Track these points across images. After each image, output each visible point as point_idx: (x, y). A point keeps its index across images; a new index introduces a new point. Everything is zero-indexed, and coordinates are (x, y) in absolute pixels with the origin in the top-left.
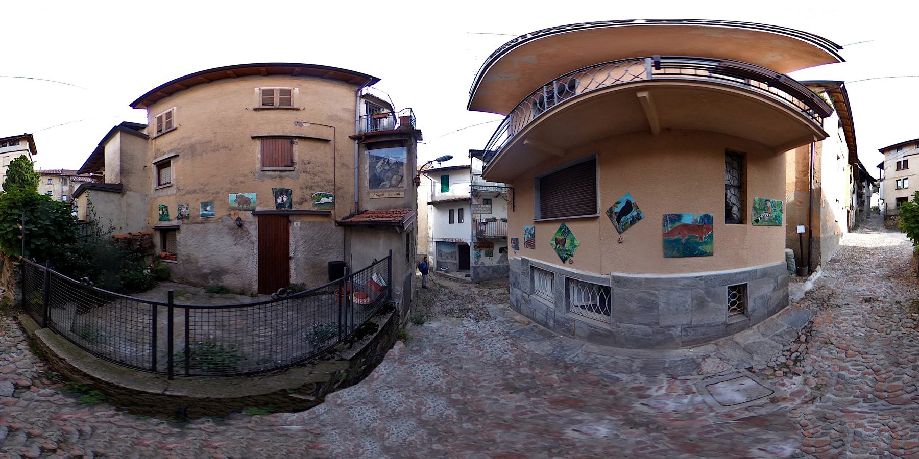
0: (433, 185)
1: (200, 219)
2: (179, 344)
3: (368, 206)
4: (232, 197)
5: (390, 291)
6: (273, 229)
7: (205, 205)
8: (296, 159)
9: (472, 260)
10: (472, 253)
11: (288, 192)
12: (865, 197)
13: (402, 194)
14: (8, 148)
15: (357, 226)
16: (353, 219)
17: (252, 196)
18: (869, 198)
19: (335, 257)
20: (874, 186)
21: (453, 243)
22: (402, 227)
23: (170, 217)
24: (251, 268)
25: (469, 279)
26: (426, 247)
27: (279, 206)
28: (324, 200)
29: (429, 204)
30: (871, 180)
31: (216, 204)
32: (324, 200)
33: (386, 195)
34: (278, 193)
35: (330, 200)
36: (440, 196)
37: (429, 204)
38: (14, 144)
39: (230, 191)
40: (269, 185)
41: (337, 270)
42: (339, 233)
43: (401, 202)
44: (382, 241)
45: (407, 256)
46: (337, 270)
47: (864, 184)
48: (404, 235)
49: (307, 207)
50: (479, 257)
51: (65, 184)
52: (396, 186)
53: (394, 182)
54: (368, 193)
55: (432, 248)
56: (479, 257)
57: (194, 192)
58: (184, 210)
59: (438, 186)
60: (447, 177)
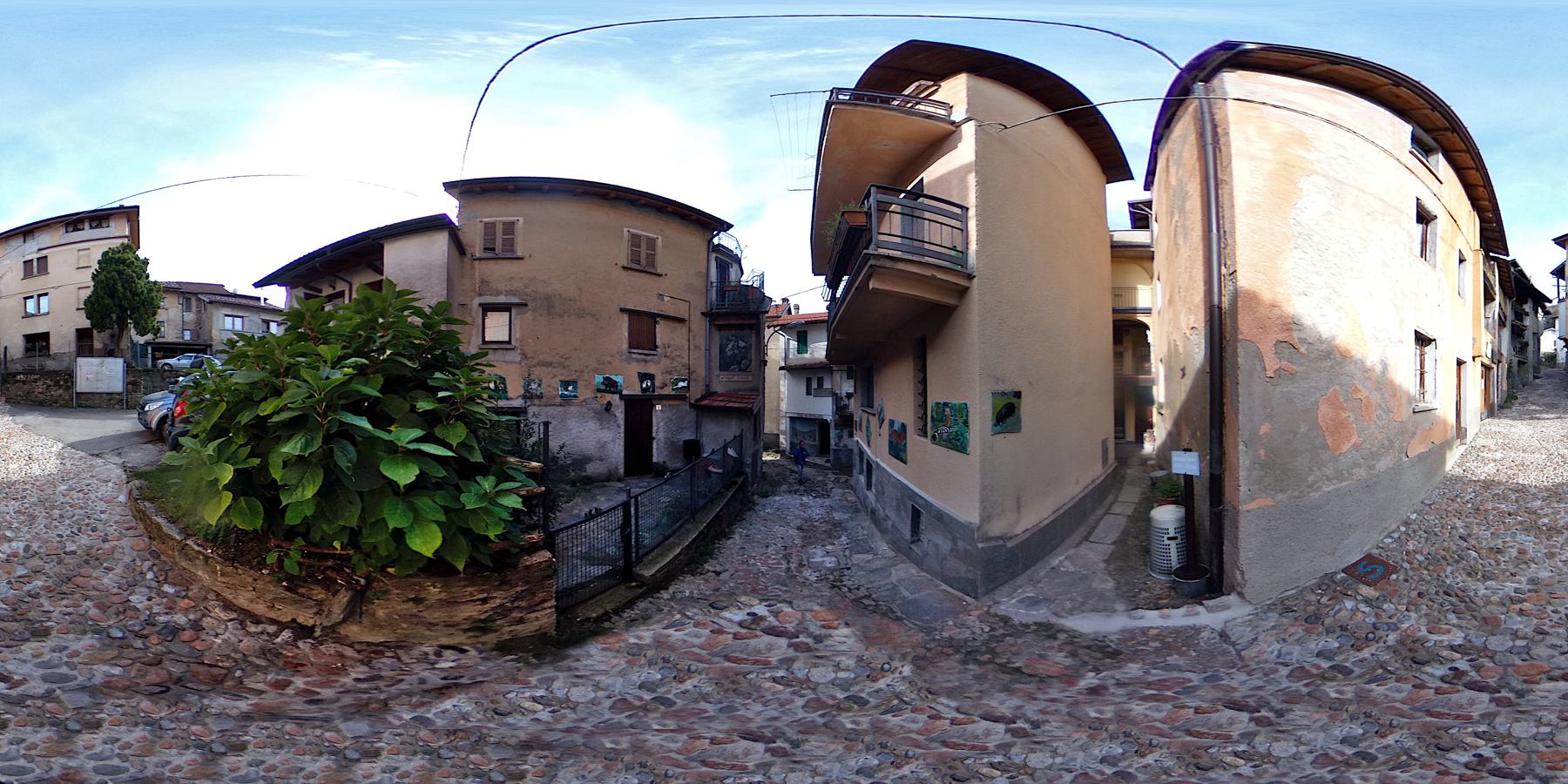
1: (558, 400)
2: (927, 215)
3: (718, 388)
4: (599, 379)
6: (638, 411)
7: (565, 384)
8: (659, 342)
9: (832, 442)
10: (833, 433)
11: (651, 377)
12: (1528, 336)
14: (87, 232)
15: (706, 408)
17: (619, 379)
18: (1537, 336)
19: (688, 435)
20: (1546, 313)
22: (751, 410)
23: (510, 395)
24: (617, 451)
26: (777, 424)
27: (644, 390)
28: (681, 384)
30: (1540, 299)
31: (580, 383)
32: (681, 384)
34: (643, 377)
38: (99, 226)
39: (596, 371)
40: (635, 369)
41: (691, 449)
42: (691, 416)
43: (749, 386)
46: (691, 449)
47: (1528, 307)
49: (668, 391)
50: (840, 437)
51: (188, 309)
55: (784, 425)
56: (840, 437)
57: (550, 364)
58: (534, 386)
59: (794, 344)
60: (805, 333)
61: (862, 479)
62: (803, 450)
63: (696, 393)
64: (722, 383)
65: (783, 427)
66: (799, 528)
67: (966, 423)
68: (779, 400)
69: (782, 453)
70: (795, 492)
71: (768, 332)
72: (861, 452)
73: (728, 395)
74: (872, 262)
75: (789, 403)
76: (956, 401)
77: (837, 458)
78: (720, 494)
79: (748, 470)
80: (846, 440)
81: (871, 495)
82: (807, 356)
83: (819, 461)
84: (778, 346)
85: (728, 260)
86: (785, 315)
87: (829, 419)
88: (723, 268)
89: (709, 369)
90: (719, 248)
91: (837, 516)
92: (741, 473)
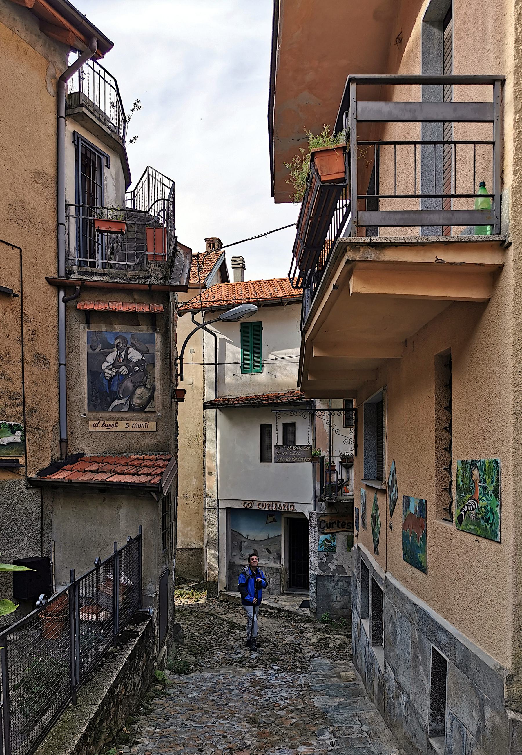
0: (219, 351)
3: (88, 449)
5: (140, 594)
9: (314, 560)
10: (315, 541)
13: (152, 425)
16: (59, 476)
21: (271, 514)
25: (307, 611)
29: (207, 406)
33: (122, 426)
35: (17, 438)
36: (238, 384)
37: (207, 406)
43: (150, 441)
44: (123, 512)
45: (164, 535)
48: (161, 502)
50: (329, 550)
52: (141, 409)
53: (136, 401)
54: (86, 420)
55: (216, 526)
59: (234, 352)
60: (258, 327)
61: (366, 624)
62: (255, 572)
63: (38, 459)
64: (100, 432)
65: (212, 531)
66: (252, 721)
67: (497, 493)
68: (203, 471)
69: (212, 588)
70: (242, 662)
71: (183, 325)
72: (365, 569)
73: (110, 458)
74: (349, 255)
75: (224, 480)
76: (486, 459)
77: (325, 598)
78: (108, 657)
79: (153, 610)
80: (342, 558)
81: (378, 654)
82: (261, 378)
83: (287, 603)
84: (204, 356)
85: (99, 143)
86: (213, 280)
87: (307, 510)
88: (89, 166)
89: (66, 405)
90: (76, 108)
91: (318, 701)
92: (140, 617)
